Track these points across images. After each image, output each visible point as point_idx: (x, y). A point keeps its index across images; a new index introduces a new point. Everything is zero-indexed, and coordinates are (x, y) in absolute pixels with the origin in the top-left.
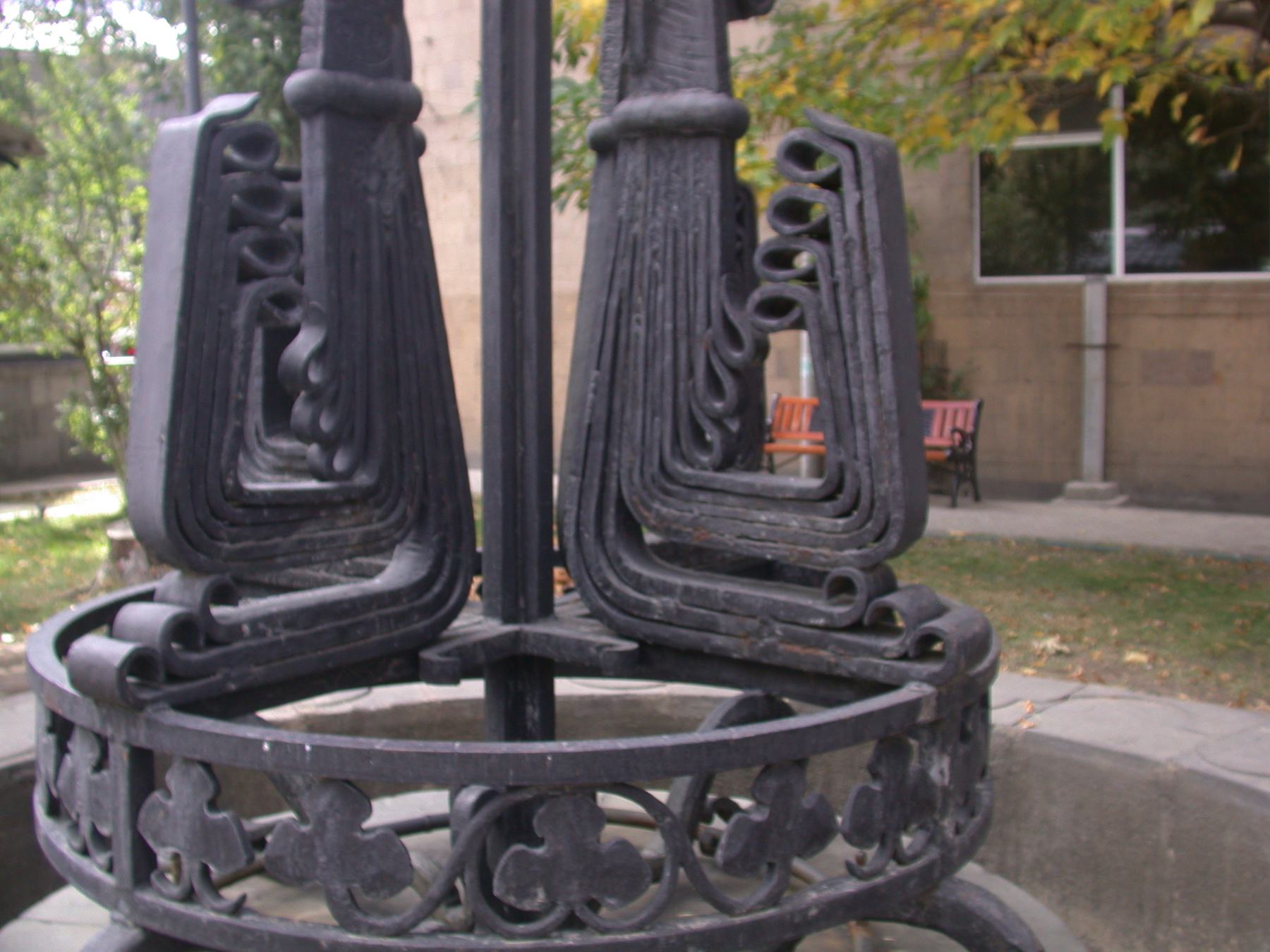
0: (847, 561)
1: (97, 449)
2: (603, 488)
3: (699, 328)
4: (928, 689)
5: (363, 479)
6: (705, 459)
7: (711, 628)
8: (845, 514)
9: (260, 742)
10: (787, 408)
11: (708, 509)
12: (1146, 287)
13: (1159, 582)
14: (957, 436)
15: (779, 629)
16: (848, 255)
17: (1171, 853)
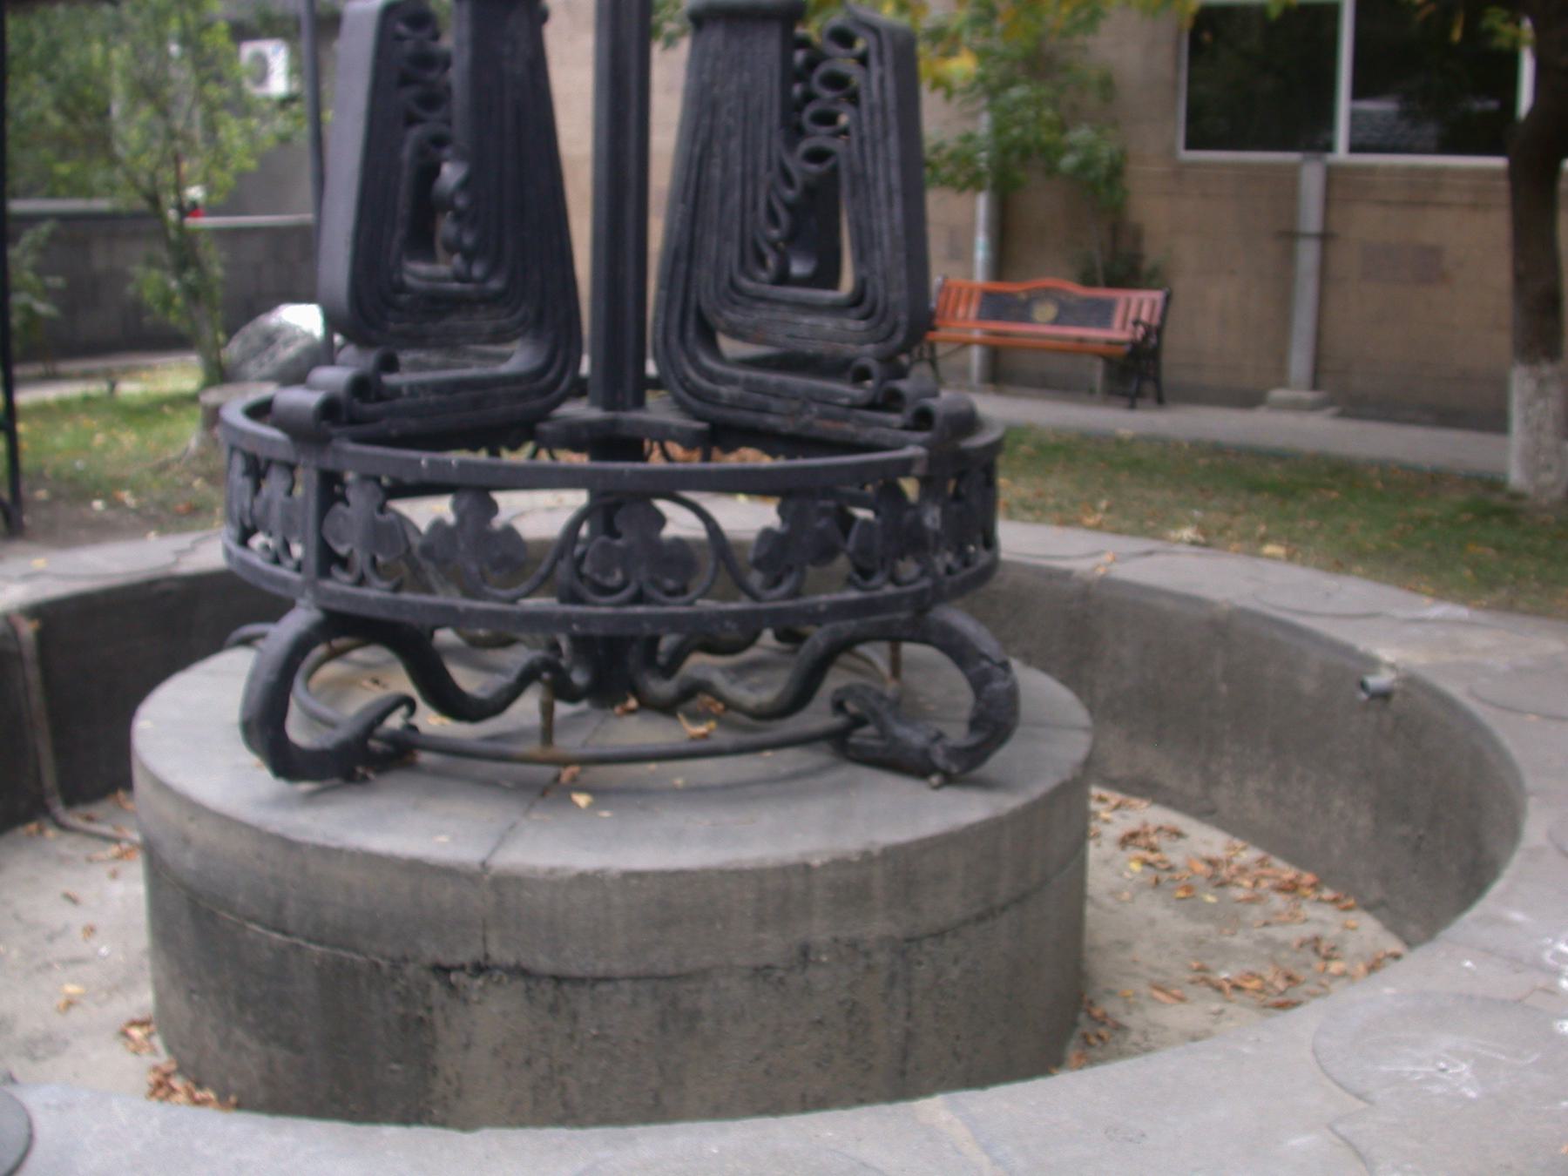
0: (867, 354)
1: (173, 318)
2: (686, 300)
3: (762, 171)
4: (921, 451)
5: (495, 284)
6: (763, 275)
7: (763, 409)
8: (865, 317)
9: (419, 461)
10: (953, 295)
11: (765, 315)
12: (1370, 170)
13: (1330, 487)
14: (1141, 330)
15: (815, 409)
16: (872, 114)
17: (1223, 688)
